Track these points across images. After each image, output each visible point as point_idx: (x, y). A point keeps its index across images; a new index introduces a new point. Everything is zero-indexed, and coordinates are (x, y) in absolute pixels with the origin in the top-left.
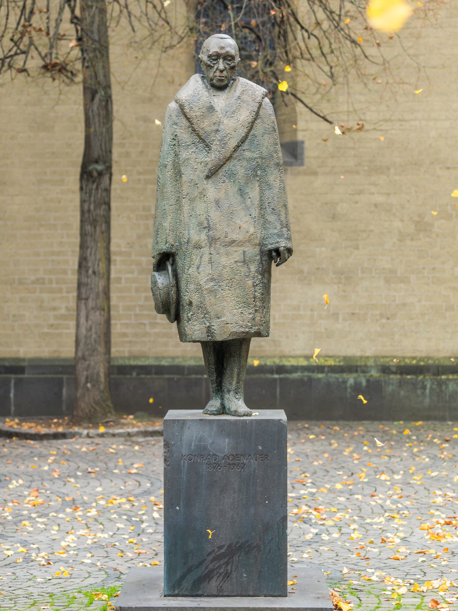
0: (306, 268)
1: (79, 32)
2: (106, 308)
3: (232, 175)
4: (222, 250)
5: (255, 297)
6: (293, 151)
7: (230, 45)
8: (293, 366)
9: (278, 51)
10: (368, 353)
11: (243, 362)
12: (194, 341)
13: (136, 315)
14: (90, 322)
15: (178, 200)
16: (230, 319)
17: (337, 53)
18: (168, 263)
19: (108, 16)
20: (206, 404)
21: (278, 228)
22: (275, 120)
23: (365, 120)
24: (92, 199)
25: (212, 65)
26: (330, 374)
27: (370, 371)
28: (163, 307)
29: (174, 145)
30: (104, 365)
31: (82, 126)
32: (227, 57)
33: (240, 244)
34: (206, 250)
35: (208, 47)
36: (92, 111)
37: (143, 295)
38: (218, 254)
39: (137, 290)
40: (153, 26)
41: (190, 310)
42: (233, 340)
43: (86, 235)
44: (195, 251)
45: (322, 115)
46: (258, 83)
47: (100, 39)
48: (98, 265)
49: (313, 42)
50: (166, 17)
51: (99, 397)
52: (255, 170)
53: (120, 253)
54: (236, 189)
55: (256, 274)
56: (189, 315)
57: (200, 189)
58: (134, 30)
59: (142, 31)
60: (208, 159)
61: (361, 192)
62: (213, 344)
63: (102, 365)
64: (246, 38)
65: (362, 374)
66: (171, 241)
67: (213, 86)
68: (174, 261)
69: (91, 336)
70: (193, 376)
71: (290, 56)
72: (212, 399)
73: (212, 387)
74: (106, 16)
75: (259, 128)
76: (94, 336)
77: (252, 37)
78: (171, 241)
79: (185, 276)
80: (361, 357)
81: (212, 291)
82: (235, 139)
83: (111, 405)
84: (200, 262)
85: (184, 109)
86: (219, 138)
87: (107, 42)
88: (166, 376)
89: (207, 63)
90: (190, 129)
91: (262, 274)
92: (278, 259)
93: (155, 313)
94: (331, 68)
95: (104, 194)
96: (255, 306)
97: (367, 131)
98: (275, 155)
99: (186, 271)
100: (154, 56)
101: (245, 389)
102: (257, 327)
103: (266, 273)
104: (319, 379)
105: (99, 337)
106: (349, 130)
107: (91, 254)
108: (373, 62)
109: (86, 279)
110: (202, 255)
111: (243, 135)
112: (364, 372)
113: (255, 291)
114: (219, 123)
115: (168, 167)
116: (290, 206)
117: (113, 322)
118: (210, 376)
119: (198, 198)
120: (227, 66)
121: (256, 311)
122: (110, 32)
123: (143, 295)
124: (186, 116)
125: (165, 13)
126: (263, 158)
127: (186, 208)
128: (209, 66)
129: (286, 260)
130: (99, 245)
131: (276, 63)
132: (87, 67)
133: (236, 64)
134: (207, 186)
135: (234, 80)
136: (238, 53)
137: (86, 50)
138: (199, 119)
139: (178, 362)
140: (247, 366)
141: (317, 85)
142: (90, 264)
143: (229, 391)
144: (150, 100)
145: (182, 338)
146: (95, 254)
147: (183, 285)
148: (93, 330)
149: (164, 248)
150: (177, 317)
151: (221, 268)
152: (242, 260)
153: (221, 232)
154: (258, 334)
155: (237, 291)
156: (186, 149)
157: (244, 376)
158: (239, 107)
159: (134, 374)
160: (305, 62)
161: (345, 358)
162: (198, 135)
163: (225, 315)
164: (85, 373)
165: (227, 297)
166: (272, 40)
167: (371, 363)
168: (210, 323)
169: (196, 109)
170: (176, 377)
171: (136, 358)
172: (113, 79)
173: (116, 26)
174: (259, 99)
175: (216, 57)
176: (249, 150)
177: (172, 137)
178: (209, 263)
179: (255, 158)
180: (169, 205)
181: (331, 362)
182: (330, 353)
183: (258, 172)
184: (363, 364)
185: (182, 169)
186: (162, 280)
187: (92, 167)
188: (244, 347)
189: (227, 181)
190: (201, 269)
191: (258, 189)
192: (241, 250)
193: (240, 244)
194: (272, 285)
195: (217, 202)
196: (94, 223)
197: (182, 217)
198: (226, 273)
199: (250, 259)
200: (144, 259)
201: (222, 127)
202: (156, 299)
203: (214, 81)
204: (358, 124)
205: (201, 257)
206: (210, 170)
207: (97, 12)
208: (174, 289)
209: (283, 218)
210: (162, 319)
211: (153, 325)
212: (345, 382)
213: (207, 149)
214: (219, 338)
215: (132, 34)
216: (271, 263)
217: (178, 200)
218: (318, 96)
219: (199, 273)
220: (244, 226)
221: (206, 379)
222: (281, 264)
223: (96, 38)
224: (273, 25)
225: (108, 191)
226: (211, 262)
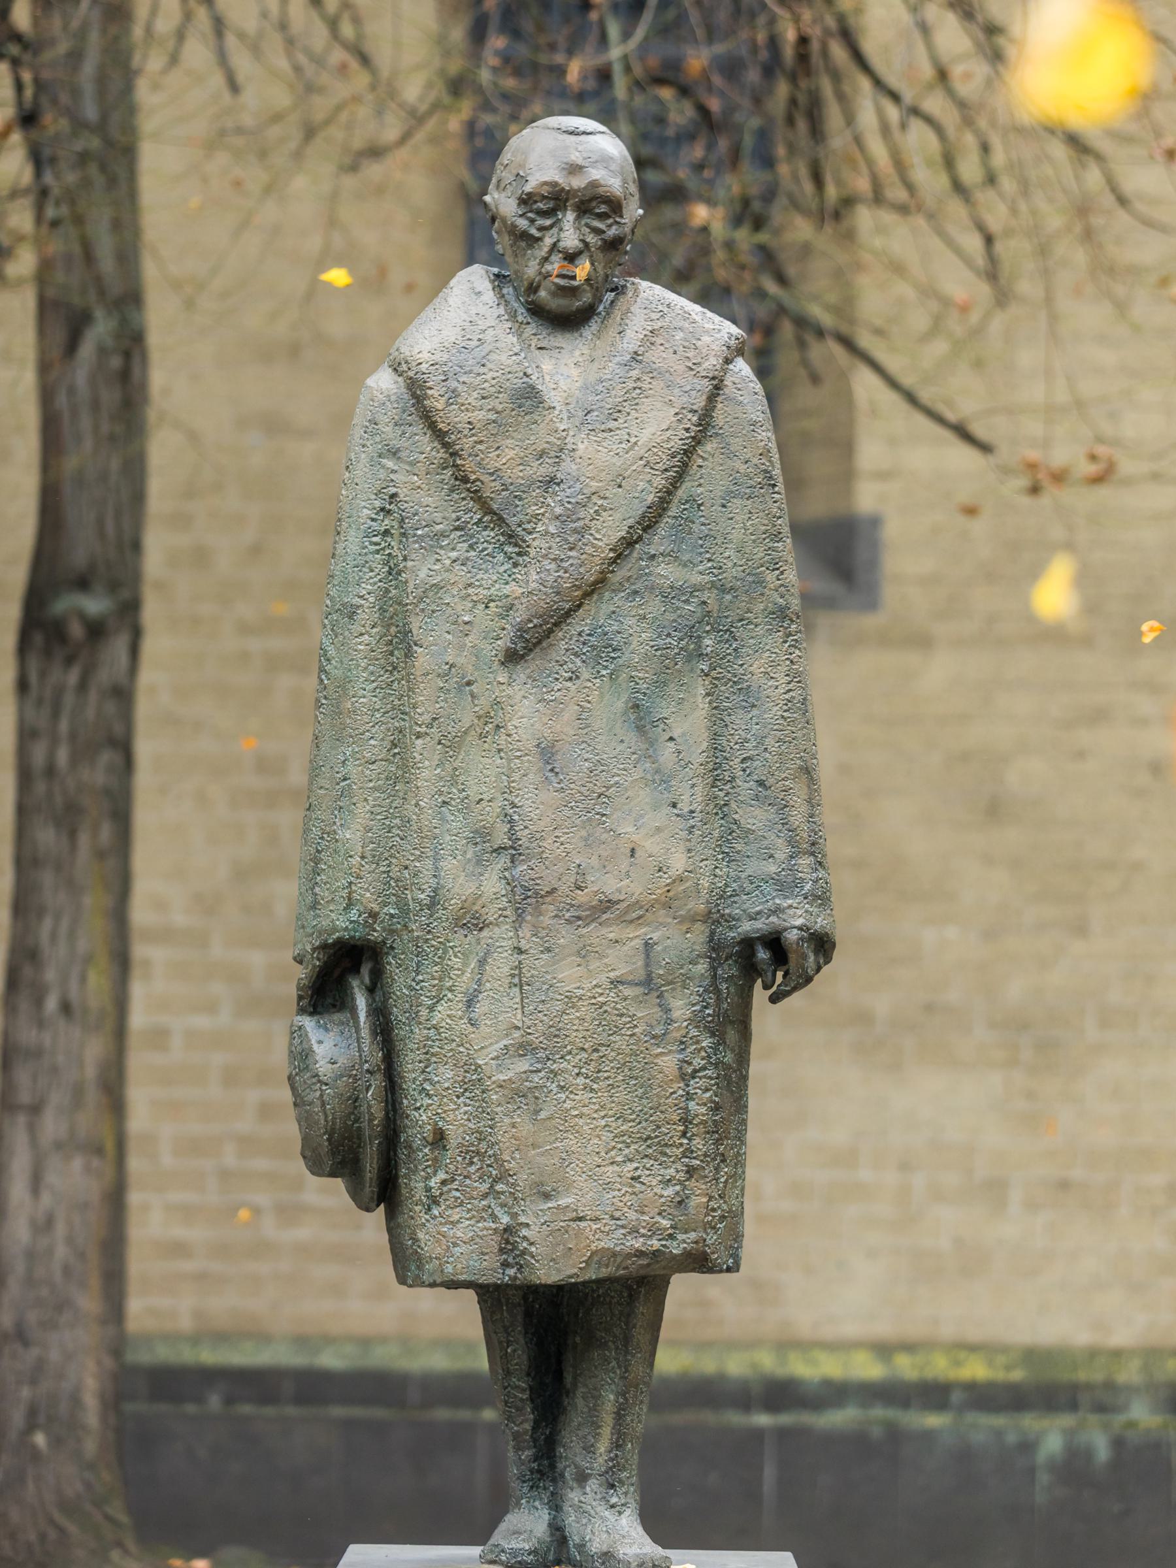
0: (882, 1005)
1: (29, 93)
2: (110, 1146)
3: (604, 651)
4: (565, 937)
5: (686, 1120)
6: (839, 554)
7: (604, 160)
8: (827, 1383)
9: (783, 169)
10: (1121, 1337)
11: (637, 1369)
12: (453, 1285)
13: (225, 1175)
14: (46, 1199)
15: (397, 745)
16: (589, 1201)
17: (1007, 184)
18: (355, 983)
19: (138, 31)
20: (495, 1527)
21: (780, 856)
22: (773, 446)
23: (1116, 442)
24: (64, 726)
25: (534, 231)
26: (971, 1417)
27: (1125, 1408)
28: (333, 1152)
29: (387, 532)
30: (99, 1363)
31: (26, 447)
32: (594, 204)
33: (633, 913)
34: (501, 935)
35: (522, 166)
36: (72, 391)
37: (253, 1096)
38: (548, 950)
39: (231, 1078)
40: (310, 69)
41: (436, 1164)
42: (599, 1282)
43: (36, 862)
44: (459, 939)
45: (951, 417)
46: (704, 298)
47: (104, 117)
48: (83, 979)
49: (919, 141)
50: (360, 36)
51: (79, 1487)
52: (692, 633)
53: (166, 935)
54: (620, 705)
55: (694, 1032)
56: (433, 1183)
57: (484, 702)
58: (234, 86)
59: (266, 90)
60: (513, 589)
61: (1098, 716)
62: (525, 1298)
63: (91, 1365)
64: (661, 120)
65: (1093, 1419)
66: (367, 896)
67: (537, 311)
68: (378, 974)
69: (50, 1251)
70: (443, 1414)
71: (831, 191)
72: (518, 1505)
73: (517, 1461)
74: (127, 31)
75: (711, 475)
76: (61, 1252)
77: (681, 114)
78: (367, 896)
79: (419, 1033)
80: (1093, 1353)
81: (519, 1093)
82: (618, 516)
83: (124, 1518)
84: (479, 982)
85: (426, 397)
86: (558, 510)
87: (130, 129)
88: (338, 1411)
89: (514, 226)
90: (449, 473)
91: (716, 1031)
92: (780, 975)
93: (301, 1165)
94: (989, 240)
95: (111, 708)
96: (688, 1153)
97: (1127, 482)
98: (770, 577)
99: (424, 1012)
100: (308, 186)
101: (641, 1466)
102: (693, 1236)
103: (731, 1027)
104: (928, 1436)
105: (82, 1256)
106: (1060, 477)
107: (54, 936)
108: (1148, 223)
109: (34, 1032)
110: (488, 953)
111: (650, 498)
112: (1101, 1408)
113: (689, 1097)
114: (560, 452)
115: (361, 616)
116: (826, 770)
117: (134, 1198)
118: (510, 1418)
119: (472, 737)
120: (591, 239)
121: (691, 1172)
122: (144, 94)
123: (253, 1096)
124: (432, 426)
125: (356, 21)
126: (723, 590)
127: (426, 774)
128: (524, 236)
129: (809, 980)
130: (88, 900)
131: (777, 214)
132: (55, 224)
133: (627, 229)
134: (509, 691)
135: (619, 290)
136: (633, 188)
137: (53, 160)
138: (481, 436)
139: (385, 1357)
140: (654, 1381)
141: (934, 306)
142: (50, 975)
143: (582, 1478)
144: (294, 351)
145: (406, 1268)
146: (72, 935)
147: (410, 1067)
148: (60, 1229)
149: (341, 923)
150: (386, 1192)
151: (559, 1006)
152: (641, 975)
153: (560, 868)
154: (698, 1262)
155: (621, 1095)
156: (430, 549)
157: (641, 1420)
158: (635, 395)
159: (214, 1401)
160: (888, 217)
161: (1031, 1356)
162: (478, 497)
163: (569, 1186)
164: (26, 1392)
165: (580, 1116)
166: (764, 136)
167: (1129, 1374)
168: (514, 1216)
169: (473, 399)
170: (379, 1413)
171: (221, 1338)
172: (150, 271)
173: (165, 71)
174: (712, 363)
175: (552, 202)
176: (672, 556)
177: (378, 504)
178: (512, 985)
179: (697, 588)
180: (361, 761)
181: (976, 1370)
182: (974, 1334)
183: (704, 640)
184: (1098, 1376)
185: (415, 624)
186: (331, 1047)
187: (66, 604)
188: (642, 1309)
189: (585, 674)
190: (480, 1009)
191: (703, 706)
192: (635, 936)
193: (633, 913)
194: (756, 1068)
195: (547, 753)
196: (69, 818)
197: (410, 810)
198: (578, 1025)
199: (670, 972)
200: (257, 959)
201: (569, 466)
202: (305, 1120)
203: (543, 293)
204: (1093, 458)
205: (482, 962)
206: (521, 630)
207: (96, 15)
208: (377, 1083)
209: (797, 817)
210: (333, 1193)
211: (289, 1213)
212: (1028, 1446)
213: (509, 549)
214: (546, 1274)
215: (227, 96)
216: (751, 988)
217: (397, 745)
218: (939, 347)
219: (472, 1023)
220: (650, 845)
221: (491, 1427)
222: (787, 994)
223: (91, 112)
224: (769, 71)
225: (123, 695)
226: (518, 979)
